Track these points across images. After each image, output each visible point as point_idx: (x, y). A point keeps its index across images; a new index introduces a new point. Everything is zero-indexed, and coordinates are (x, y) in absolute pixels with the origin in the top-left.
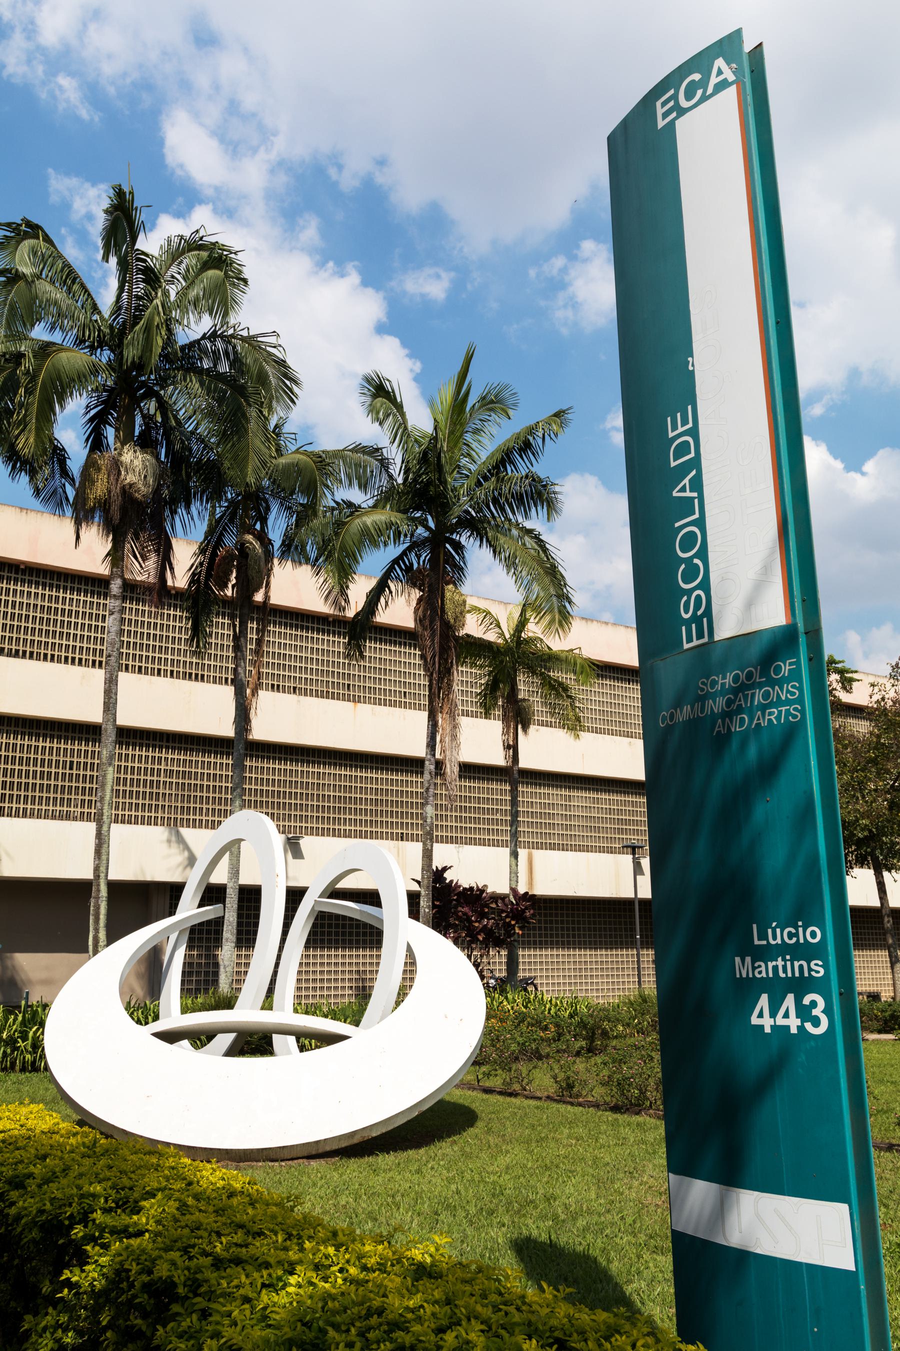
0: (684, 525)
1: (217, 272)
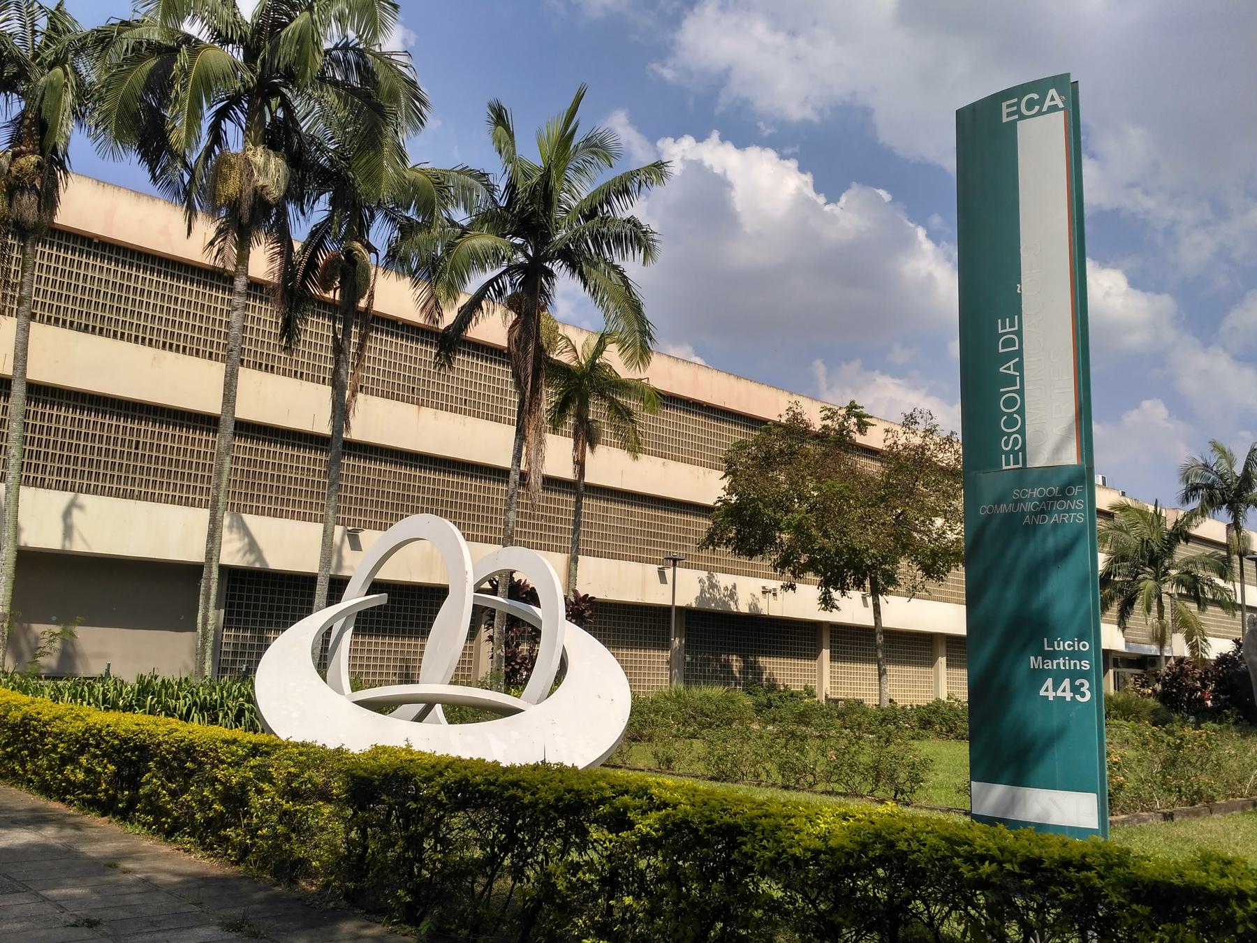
0: (1007, 392)
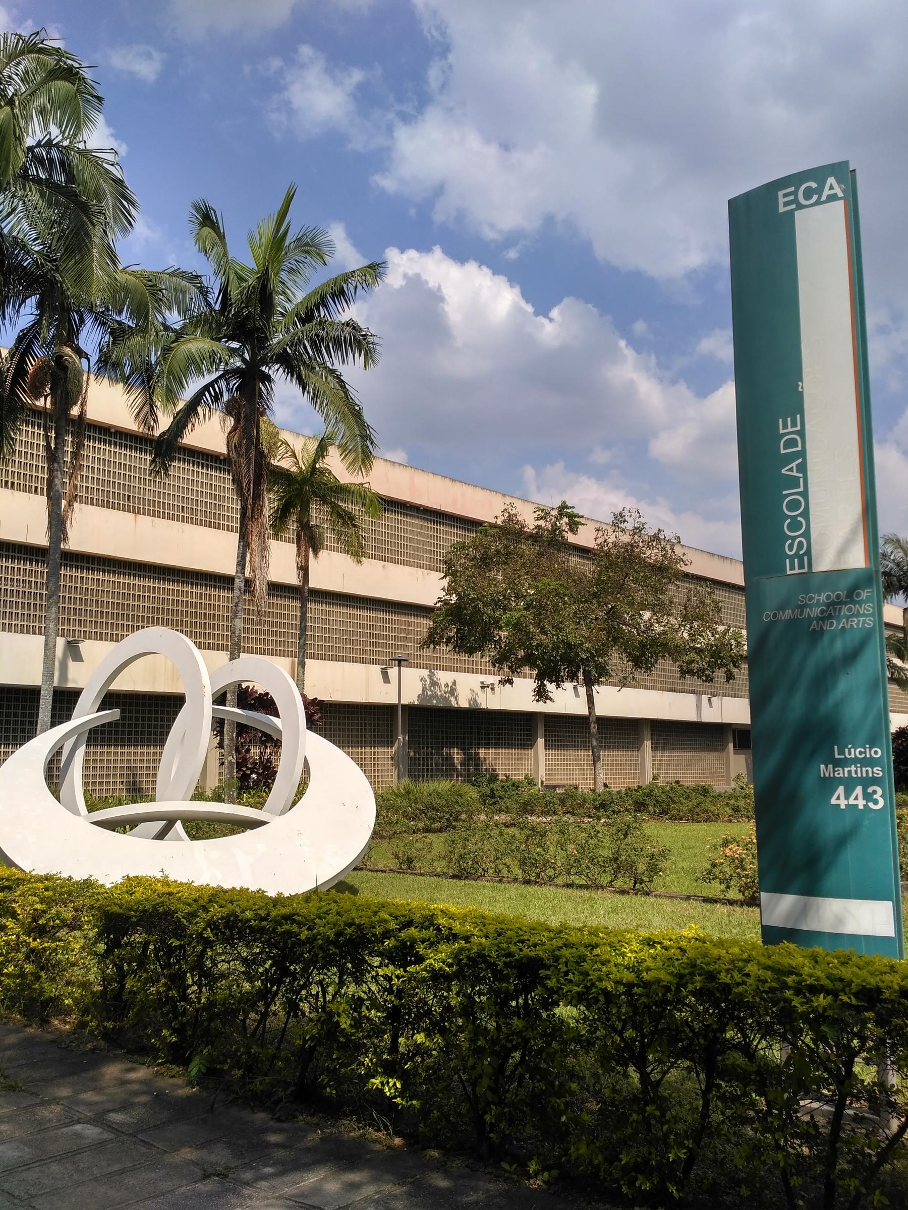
1: (67, 85)
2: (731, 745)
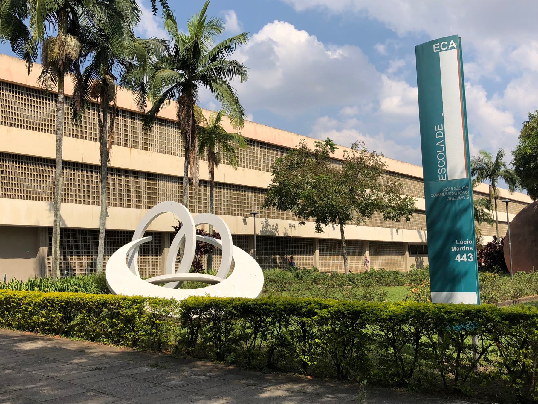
0: (440, 152)
2: (407, 253)
